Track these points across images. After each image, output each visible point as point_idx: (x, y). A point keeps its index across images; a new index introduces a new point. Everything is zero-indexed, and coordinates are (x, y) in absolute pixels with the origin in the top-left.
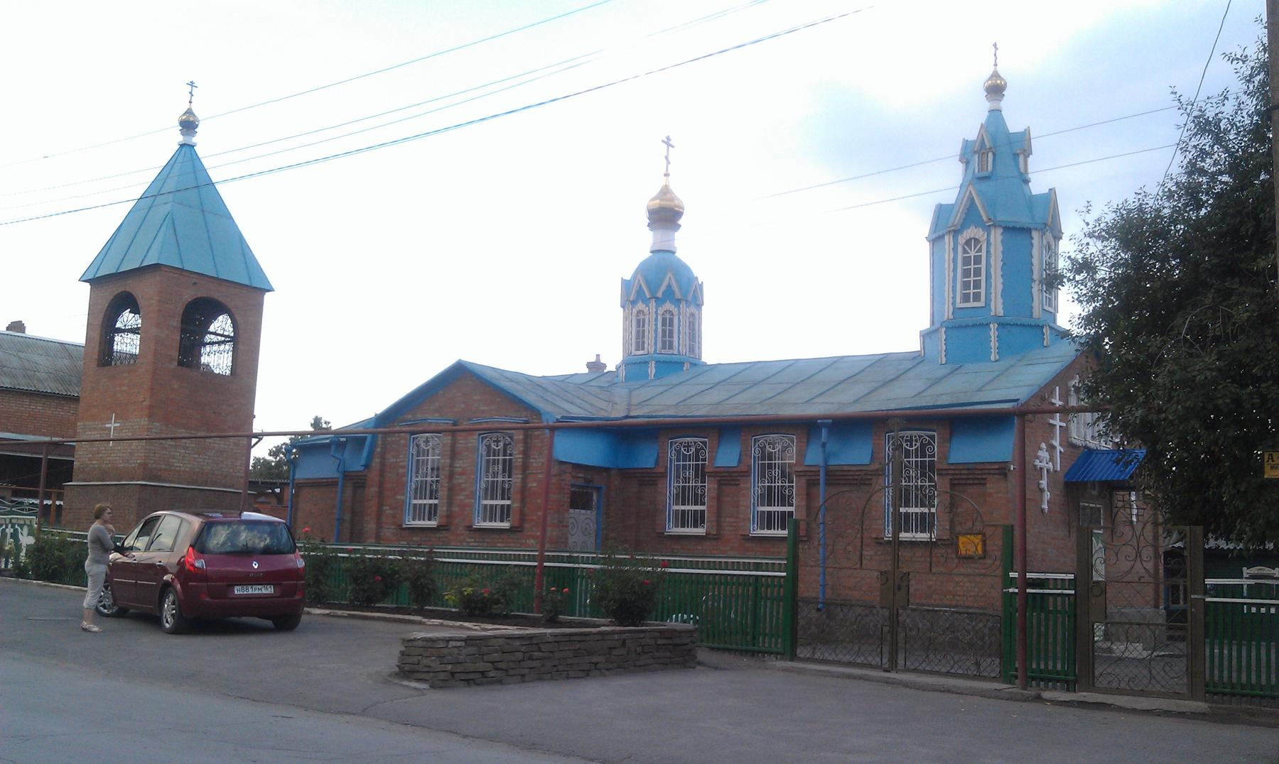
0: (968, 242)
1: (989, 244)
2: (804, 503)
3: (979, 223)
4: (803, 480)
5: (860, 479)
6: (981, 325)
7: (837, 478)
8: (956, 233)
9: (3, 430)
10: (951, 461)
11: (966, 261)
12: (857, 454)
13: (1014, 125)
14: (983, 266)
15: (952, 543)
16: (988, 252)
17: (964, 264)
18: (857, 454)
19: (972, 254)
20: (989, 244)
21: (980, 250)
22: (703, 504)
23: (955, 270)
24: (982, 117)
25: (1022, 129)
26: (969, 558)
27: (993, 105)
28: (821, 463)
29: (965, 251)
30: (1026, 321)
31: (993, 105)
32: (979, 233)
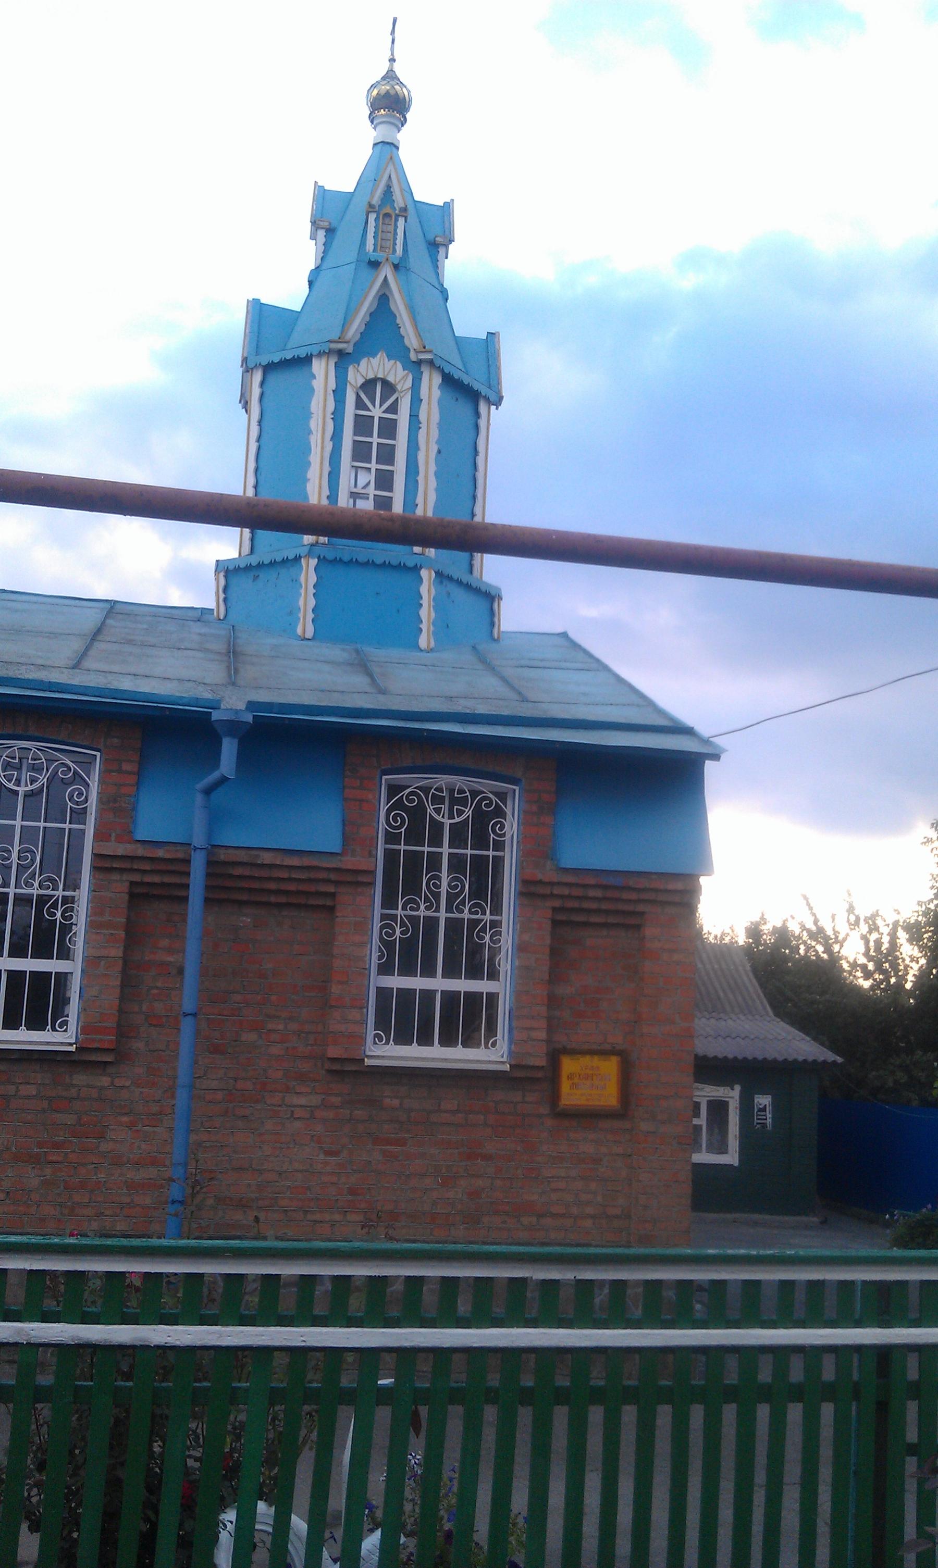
0: (368, 385)
1: (416, 401)
2: (117, 952)
3: (399, 351)
4: (120, 886)
5: (308, 893)
6: (285, 562)
7: (238, 884)
8: (343, 358)
9: (9, 1316)
10: (142, 833)
11: (363, 425)
12: (305, 824)
13: (426, 188)
14: (401, 442)
15: (550, 1076)
16: (414, 417)
17: (357, 430)
18: (305, 824)
19: (377, 412)
20: (416, 401)
21: (393, 409)
22: (383, 994)
23: (337, 437)
24: (364, 152)
25: (438, 200)
26: (588, 1117)
27: (383, 133)
28: (199, 840)
29: (360, 404)
30: (465, 578)
31: (383, 133)
32: (396, 373)
